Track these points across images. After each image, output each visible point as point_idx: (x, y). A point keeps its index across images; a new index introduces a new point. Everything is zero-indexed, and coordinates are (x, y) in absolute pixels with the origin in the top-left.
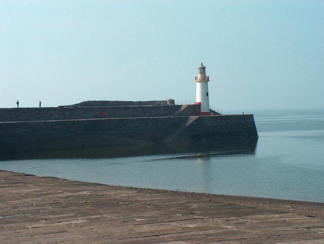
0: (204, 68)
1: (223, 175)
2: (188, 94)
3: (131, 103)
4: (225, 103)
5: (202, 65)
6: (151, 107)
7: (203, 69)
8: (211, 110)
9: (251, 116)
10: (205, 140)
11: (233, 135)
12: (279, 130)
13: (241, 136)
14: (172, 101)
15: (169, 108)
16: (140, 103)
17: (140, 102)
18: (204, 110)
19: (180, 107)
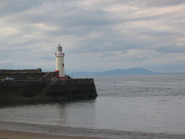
0: (61, 48)
1: (76, 115)
2: (49, 66)
3: (12, 71)
4: (75, 68)
5: (60, 46)
6: (26, 73)
7: (60, 49)
8: (65, 75)
9: (92, 79)
10: (26, 77)
11: (82, 91)
12: (22, 123)
13: (86, 93)
14: (40, 70)
15: (38, 73)
16: (18, 71)
17: (18, 70)
18: (61, 75)
19: (44, 73)
